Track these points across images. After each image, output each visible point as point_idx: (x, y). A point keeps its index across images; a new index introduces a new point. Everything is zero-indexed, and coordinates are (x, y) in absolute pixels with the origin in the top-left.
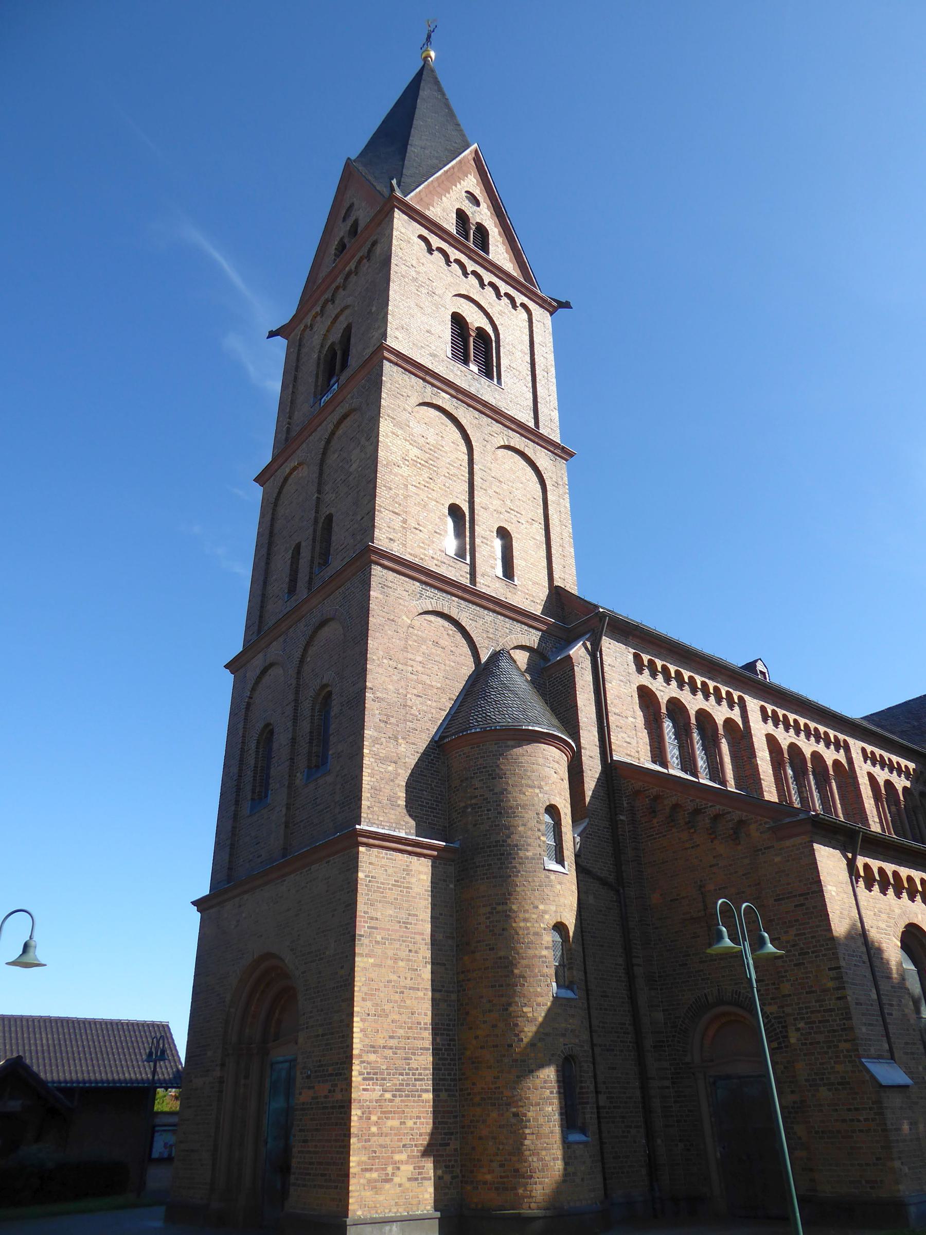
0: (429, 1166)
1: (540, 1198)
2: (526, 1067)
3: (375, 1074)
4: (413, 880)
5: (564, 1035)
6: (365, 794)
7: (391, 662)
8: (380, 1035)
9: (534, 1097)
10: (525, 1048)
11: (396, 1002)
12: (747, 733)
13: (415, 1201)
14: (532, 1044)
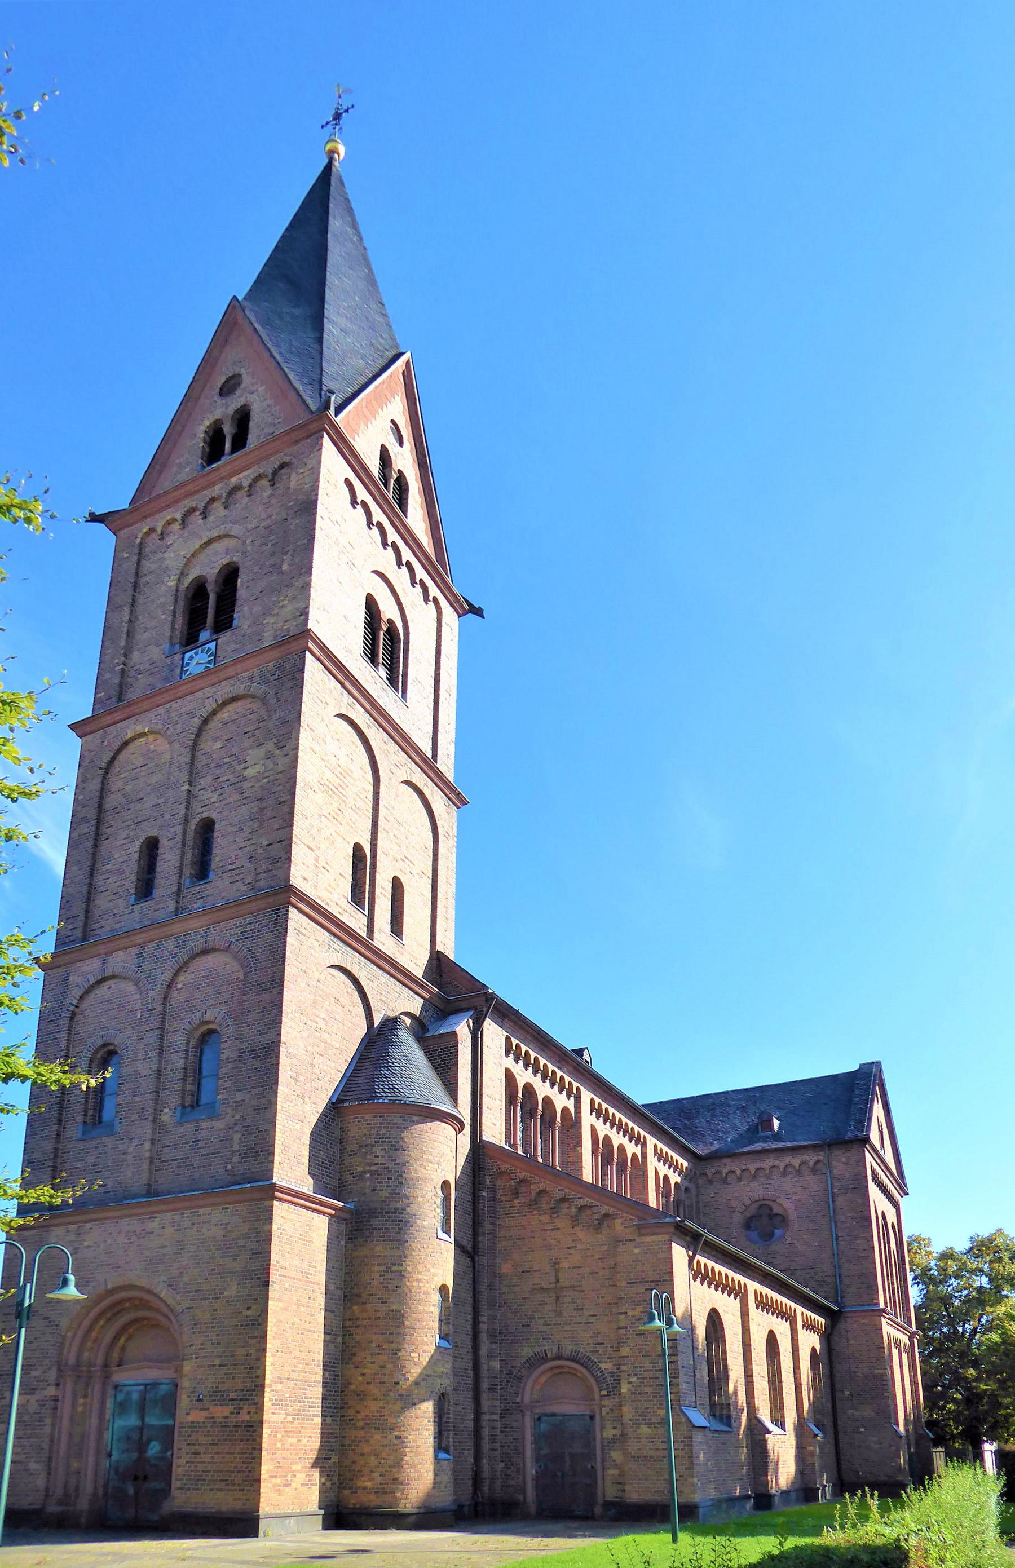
0: (316, 1474)
1: (414, 1500)
2: (409, 1401)
3: (281, 1400)
4: (314, 1235)
5: (440, 1377)
6: (278, 1150)
7: (302, 1017)
8: (285, 1368)
9: (415, 1423)
10: (410, 1386)
11: (298, 1341)
12: (578, 1122)
13: (305, 1501)
14: (416, 1383)
